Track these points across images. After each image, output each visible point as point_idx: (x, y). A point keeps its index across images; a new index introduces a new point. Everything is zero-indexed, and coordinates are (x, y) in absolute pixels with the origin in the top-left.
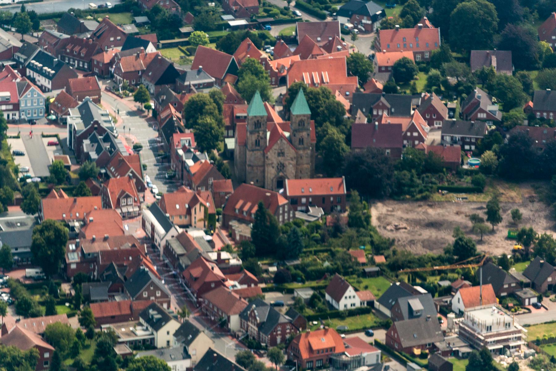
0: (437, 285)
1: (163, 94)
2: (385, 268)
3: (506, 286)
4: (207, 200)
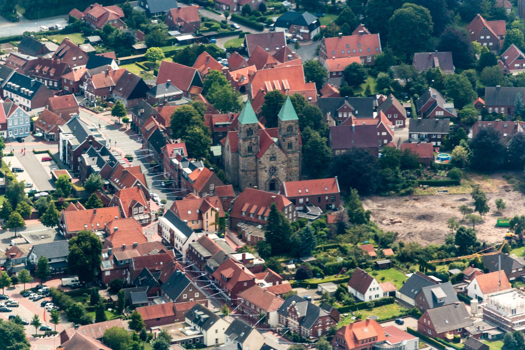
0: (448, 273)
1: (142, 108)
2: (395, 260)
3: (514, 271)
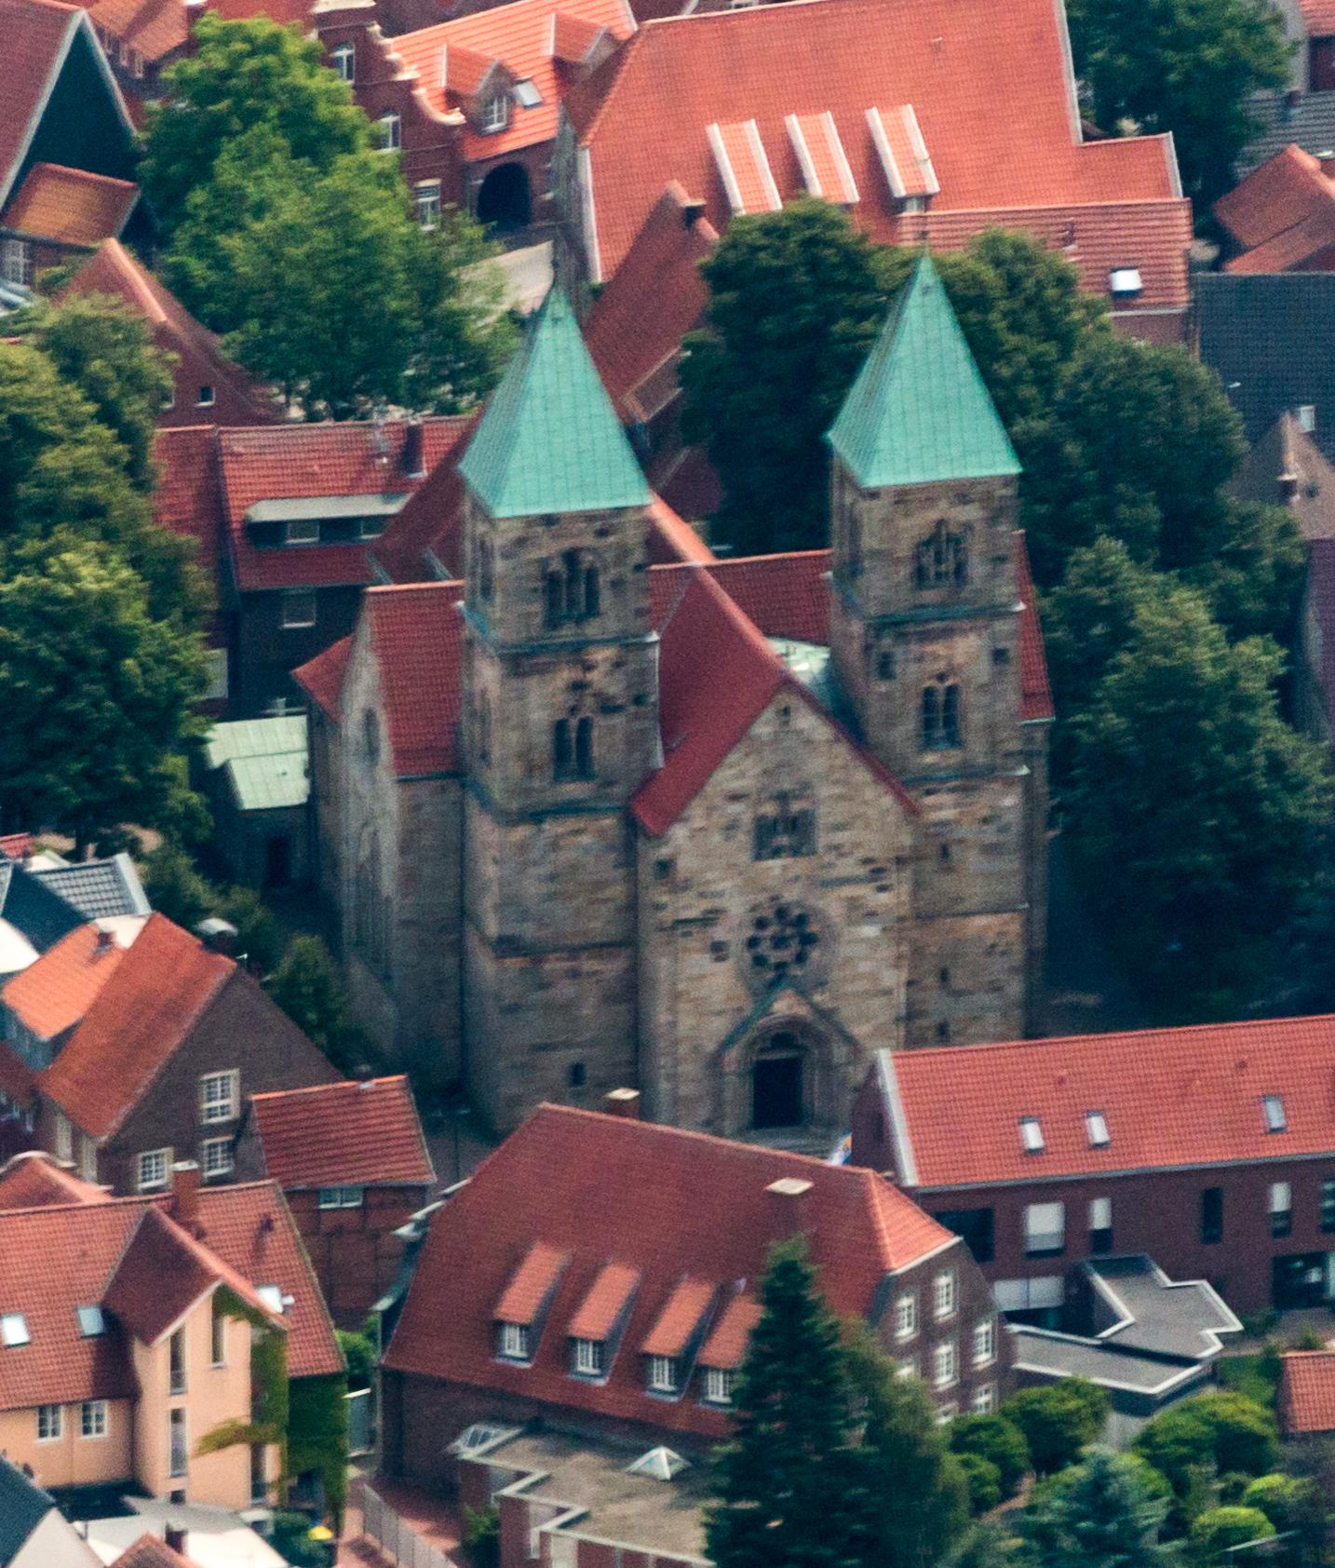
4: (257, 1266)
